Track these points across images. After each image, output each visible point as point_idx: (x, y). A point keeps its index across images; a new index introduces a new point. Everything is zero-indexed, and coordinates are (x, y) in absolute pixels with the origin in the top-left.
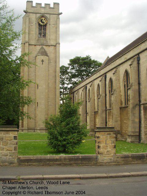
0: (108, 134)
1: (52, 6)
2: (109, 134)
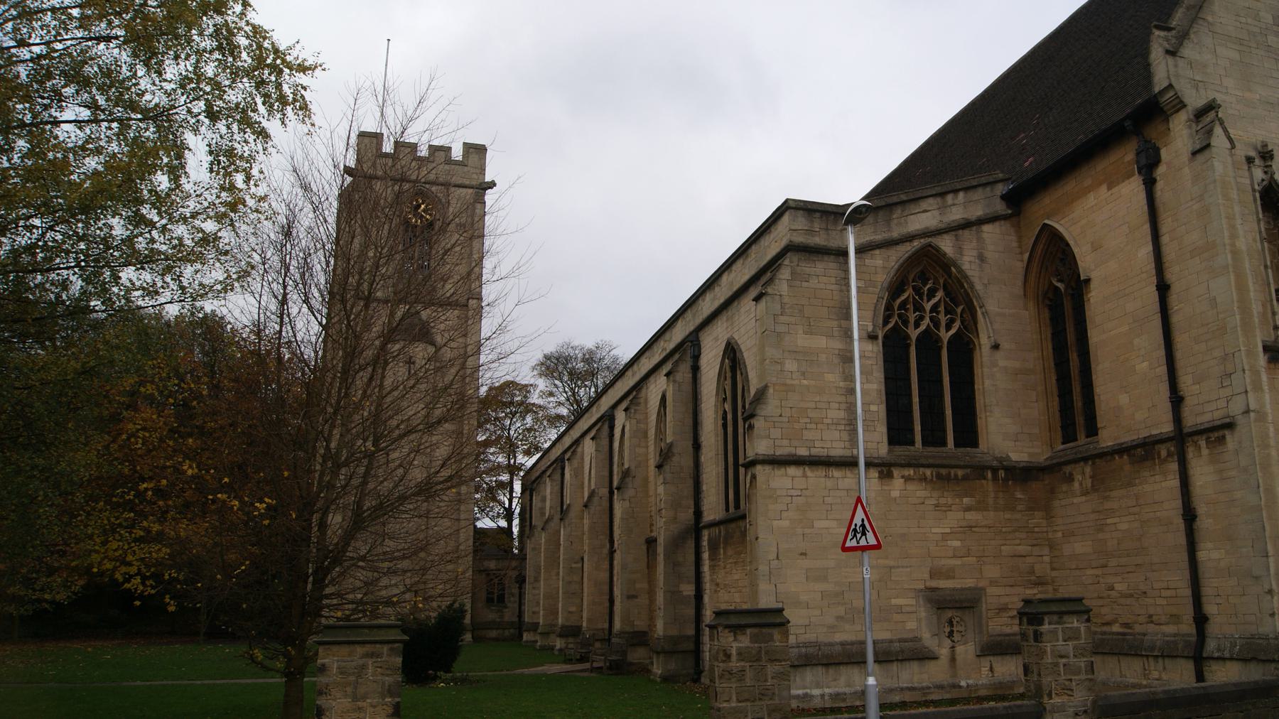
0: (367, 655)
1: (457, 153)
2: (372, 655)
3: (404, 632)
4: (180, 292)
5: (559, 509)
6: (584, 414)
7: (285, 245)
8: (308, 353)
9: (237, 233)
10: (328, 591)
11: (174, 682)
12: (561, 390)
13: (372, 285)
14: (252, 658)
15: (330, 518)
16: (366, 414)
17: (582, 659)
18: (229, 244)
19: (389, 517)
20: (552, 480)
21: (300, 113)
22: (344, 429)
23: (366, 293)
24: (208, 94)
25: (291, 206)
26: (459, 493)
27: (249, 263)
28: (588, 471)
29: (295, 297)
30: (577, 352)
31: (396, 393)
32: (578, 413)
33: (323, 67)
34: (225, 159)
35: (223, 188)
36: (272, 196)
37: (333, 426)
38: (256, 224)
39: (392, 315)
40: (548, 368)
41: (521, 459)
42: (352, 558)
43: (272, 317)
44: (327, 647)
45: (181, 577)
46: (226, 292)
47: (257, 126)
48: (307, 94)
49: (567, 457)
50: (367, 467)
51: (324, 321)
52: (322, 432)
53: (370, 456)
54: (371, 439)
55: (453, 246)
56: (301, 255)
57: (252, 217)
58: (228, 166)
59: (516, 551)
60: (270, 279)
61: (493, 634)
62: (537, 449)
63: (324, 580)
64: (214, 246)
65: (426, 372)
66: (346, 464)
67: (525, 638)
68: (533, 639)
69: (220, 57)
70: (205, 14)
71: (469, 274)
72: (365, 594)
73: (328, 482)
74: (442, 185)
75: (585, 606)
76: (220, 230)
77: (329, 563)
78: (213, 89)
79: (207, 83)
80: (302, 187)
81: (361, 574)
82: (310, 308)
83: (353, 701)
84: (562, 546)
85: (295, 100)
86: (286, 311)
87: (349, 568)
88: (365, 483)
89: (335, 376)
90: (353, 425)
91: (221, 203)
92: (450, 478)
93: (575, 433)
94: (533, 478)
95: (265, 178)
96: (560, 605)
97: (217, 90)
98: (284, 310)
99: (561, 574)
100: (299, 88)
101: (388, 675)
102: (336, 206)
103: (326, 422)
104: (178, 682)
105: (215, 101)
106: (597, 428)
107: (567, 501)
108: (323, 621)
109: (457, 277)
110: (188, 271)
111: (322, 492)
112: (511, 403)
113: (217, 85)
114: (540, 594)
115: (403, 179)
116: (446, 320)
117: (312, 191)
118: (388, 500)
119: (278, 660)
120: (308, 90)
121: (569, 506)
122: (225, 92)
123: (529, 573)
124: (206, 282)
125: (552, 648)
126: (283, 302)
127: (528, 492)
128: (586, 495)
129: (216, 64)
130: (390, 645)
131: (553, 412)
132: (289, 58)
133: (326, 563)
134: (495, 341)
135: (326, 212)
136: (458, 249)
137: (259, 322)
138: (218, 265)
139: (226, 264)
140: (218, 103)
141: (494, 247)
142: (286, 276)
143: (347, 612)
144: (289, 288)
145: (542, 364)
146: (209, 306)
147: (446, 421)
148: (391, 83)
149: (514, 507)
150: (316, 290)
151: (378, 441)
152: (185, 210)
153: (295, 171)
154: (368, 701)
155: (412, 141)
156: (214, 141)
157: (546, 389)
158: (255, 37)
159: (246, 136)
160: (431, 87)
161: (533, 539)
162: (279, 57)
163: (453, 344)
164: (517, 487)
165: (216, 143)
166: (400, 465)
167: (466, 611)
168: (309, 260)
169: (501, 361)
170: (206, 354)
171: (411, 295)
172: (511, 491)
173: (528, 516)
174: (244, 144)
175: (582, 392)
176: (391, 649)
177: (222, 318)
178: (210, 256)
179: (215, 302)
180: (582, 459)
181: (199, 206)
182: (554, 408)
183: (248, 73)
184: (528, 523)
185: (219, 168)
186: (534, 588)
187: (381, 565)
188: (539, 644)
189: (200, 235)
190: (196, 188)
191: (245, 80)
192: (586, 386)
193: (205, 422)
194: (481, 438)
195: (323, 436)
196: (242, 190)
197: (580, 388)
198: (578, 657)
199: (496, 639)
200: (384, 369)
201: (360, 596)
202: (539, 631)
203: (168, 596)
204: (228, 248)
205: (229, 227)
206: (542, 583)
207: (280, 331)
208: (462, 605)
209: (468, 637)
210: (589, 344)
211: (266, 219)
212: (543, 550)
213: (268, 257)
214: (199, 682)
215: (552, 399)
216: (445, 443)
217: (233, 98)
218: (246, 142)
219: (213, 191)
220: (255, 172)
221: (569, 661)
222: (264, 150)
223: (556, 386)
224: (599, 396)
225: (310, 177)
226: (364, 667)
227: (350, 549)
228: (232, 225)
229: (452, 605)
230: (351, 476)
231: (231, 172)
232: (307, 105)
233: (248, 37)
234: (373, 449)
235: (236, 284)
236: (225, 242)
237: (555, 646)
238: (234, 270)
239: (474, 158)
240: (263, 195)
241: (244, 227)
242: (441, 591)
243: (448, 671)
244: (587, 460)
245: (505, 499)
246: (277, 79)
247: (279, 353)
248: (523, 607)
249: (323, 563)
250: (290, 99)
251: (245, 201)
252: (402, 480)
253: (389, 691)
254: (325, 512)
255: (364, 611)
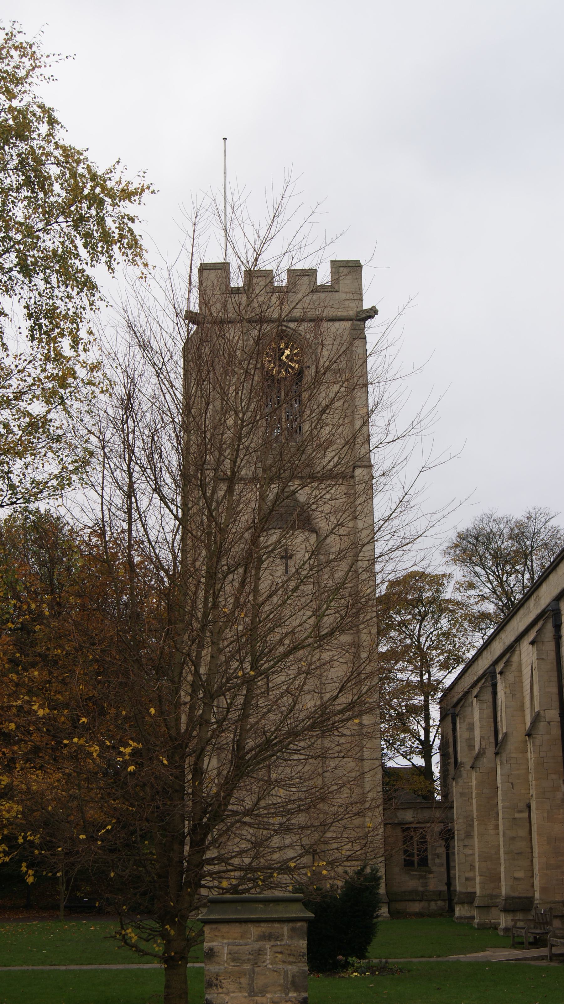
2: (268, 937)
3: (307, 904)
4: (10, 492)
5: (492, 740)
6: (518, 610)
7: (127, 422)
8: (165, 555)
9: (69, 413)
10: (209, 855)
11: (35, 968)
12: (483, 579)
13: (235, 462)
14: (124, 939)
15: (206, 762)
16: (241, 628)
17: (537, 943)
18: (61, 428)
19: (278, 758)
20: (480, 701)
21: (129, 252)
22: (215, 649)
23: (229, 474)
24: (19, 243)
25: (130, 370)
26: (361, 724)
27: (86, 449)
28: (528, 687)
29: (144, 485)
30: (502, 526)
31: (275, 599)
32: (508, 608)
33: (151, 189)
34: (46, 322)
35: (47, 358)
36: (106, 362)
37: (201, 646)
38: (90, 400)
39: (262, 498)
40: (464, 551)
41: (437, 674)
42: (235, 813)
43: (119, 513)
44: (214, 926)
45: (37, 841)
46: (63, 489)
47: (80, 275)
48: (136, 227)
49: (498, 669)
50: (246, 695)
51: (180, 515)
52: (188, 655)
53: (249, 682)
54: (249, 659)
55: (332, 401)
56: (147, 432)
57: (85, 391)
58: (53, 330)
59: (438, 798)
60: (112, 466)
61: (416, 907)
62: (458, 660)
63: (203, 840)
64: (44, 432)
65: (311, 569)
66: (221, 692)
67: (457, 914)
68: (468, 914)
69: (29, 194)
70: (7, 142)
71: (355, 436)
72: (255, 857)
73: (201, 716)
74: (311, 321)
75: (536, 871)
76: (49, 412)
77: (209, 819)
78: (24, 236)
79: (18, 231)
80: (140, 347)
81: (247, 832)
82: (163, 498)
83: (250, 996)
84: (500, 789)
85: (122, 236)
86: (134, 505)
87: (232, 825)
88: (244, 717)
89: (199, 582)
90: (226, 643)
91: (46, 377)
92: (351, 706)
93: (508, 637)
94: (455, 700)
95: (95, 340)
96: (502, 869)
97: (28, 237)
98: (131, 503)
99: (501, 828)
100: (126, 220)
101: (290, 963)
102: (182, 366)
103: (193, 641)
104: (40, 968)
105: (28, 251)
106: (537, 628)
107: (503, 728)
108: (203, 892)
109: (340, 442)
110: (18, 465)
111: (193, 729)
112: (419, 600)
113: (29, 232)
114: (473, 854)
115: (262, 320)
116: (331, 499)
117: (152, 349)
118: (276, 738)
119: (155, 942)
120: (136, 221)
121: (506, 735)
122: (38, 238)
123: (458, 827)
124: (39, 477)
125: (495, 927)
126: (130, 493)
127: (449, 719)
128: (528, 720)
129: (25, 203)
130: (291, 925)
131: (476, 609)
132: (109, 184)
133: (205, 820)
134: (396, 522)
135: (172, 375)
136: (338, 404)
137: (103, 521)
138: (50, 454)
139: (60, 453)
140: (31, 253)
141: (385, 397)
142: (130, 460)
143: (234, 882)
144: (135, 475)
145: (457, 546)
146: (42, 506)
147: (342, 632)
148: (236, 197)
149: (431, 739)
150: (168, 475)
151: (257, 661)
152: (8, 391)
153: (130, 326)
154: (269, 995)
155: (268, 268)
156: (32, 301)
157: (464, 579)
158: (67, 162)
159: (69, 289)
160: (287, 194)
161: (461, 781)
162: (97, 185)
163: (343, 531)
164: (435, 712)
165: (35, 303)
166: (287, 691)
167: (380, 878)
168: (156, 438)
169: (404, 548)
170: (42, 564)
171: (285, 471)
172: (427, 718)
173: (451, 750)
174: (67, 300)
175: (512, 580)
176: (293, 930)
177: (58, 518)
178: (41, 445)
179: (51, 502)
180: (520, 671)
181: (23, 384)
182: (476, 604)
183: (64, 210)
184: (452, 760)
185: (41, 335)
186: (465, 846)
187: (271, 820)
188: (476, 921)
189: (27, 420)
190: (17, 362)
191: (61, 219)
192: (517, 572)
193: (48, 649)
194: (383, 649)
195: (191, 660)
196: (70, 359)
197: (509, 574)
198: (531, 940)
199: (420, 915)
200: (258, 569)
201: (247, 861)
202: (476, 904)
203: (24, 864)
204: (60, 432)
205: (59, 407)
206: (476, 840)
207: (130, 530)
208: (375, 870)
209: (384, 911)
210: (519, 515)
211: (102, 392)
212: (474, 795)
213: (107, 439)
214: (63, 968)
215: (472, 592)
216: (341, 660)
217: (49, 244)
218: (69, 297)
219: (37, 364)
220: (83, 333)
221: (518, 945)
222: (91, 305)
223: (477, 575)
224: (536, 586)
225: (148, 332)
226: (260, 952)
227: (232, 800)
228: (63, 403)
229: (362, 870)
230: (228, 709)
231: (55, 337)
232: (136, 242)
233: (58, 164)
234: (252, 673)
235: (74, 477)
236: (56, 425)
237: (499, 924)
238: (70, 460)
239: (346, 283)
240: (95, 361)
241: (77, 405)
242: (348, 853)
243: (362, 956)
244: (526, 672)
245: (420, 727)
246: (98, 213)
247: (130, 555)
248: (452, 872)
249: (201, 820)
250: (116, 236)
251: (75, 372)
252: (291, 711)
253: (293, 983)
254: (200, 758)
255: (254, 880)
